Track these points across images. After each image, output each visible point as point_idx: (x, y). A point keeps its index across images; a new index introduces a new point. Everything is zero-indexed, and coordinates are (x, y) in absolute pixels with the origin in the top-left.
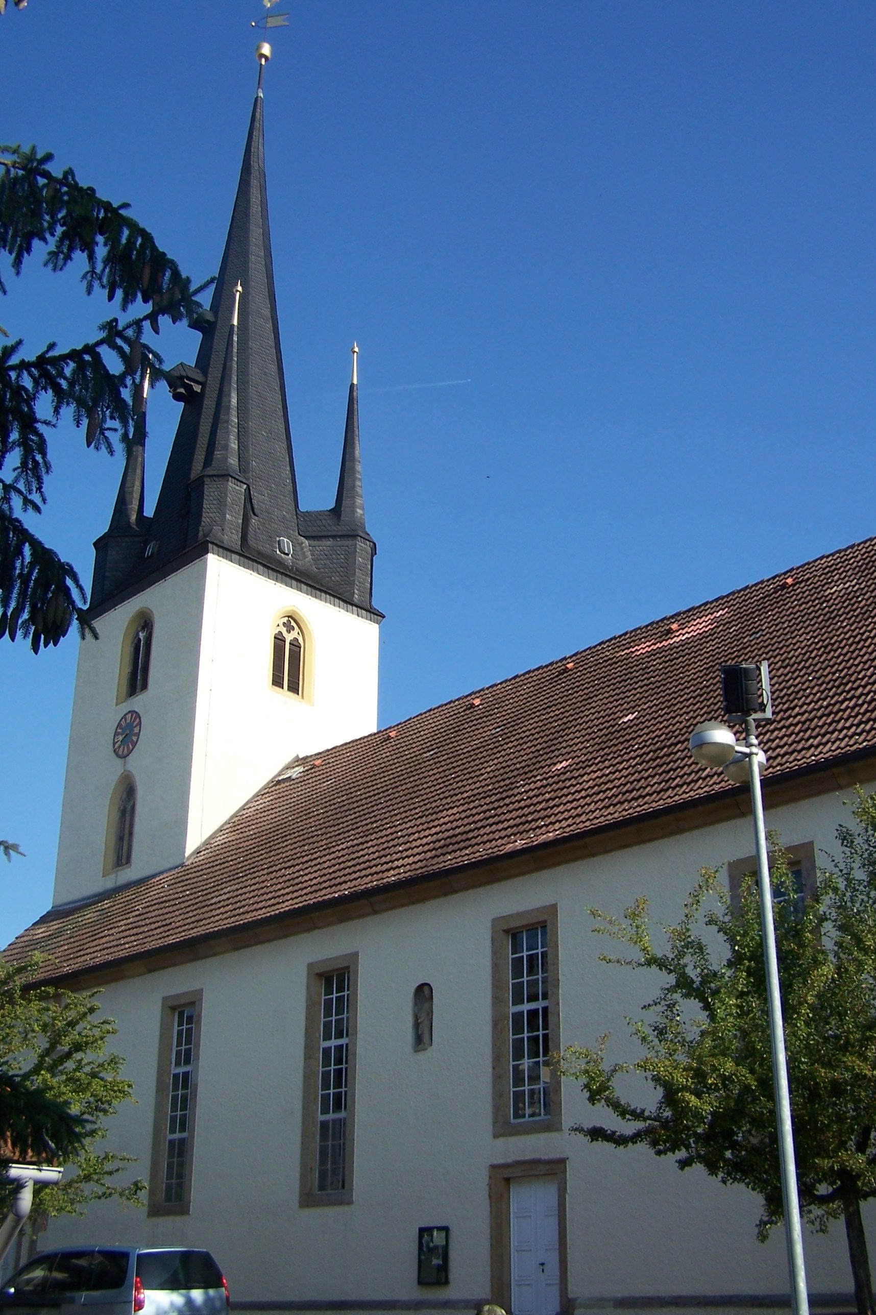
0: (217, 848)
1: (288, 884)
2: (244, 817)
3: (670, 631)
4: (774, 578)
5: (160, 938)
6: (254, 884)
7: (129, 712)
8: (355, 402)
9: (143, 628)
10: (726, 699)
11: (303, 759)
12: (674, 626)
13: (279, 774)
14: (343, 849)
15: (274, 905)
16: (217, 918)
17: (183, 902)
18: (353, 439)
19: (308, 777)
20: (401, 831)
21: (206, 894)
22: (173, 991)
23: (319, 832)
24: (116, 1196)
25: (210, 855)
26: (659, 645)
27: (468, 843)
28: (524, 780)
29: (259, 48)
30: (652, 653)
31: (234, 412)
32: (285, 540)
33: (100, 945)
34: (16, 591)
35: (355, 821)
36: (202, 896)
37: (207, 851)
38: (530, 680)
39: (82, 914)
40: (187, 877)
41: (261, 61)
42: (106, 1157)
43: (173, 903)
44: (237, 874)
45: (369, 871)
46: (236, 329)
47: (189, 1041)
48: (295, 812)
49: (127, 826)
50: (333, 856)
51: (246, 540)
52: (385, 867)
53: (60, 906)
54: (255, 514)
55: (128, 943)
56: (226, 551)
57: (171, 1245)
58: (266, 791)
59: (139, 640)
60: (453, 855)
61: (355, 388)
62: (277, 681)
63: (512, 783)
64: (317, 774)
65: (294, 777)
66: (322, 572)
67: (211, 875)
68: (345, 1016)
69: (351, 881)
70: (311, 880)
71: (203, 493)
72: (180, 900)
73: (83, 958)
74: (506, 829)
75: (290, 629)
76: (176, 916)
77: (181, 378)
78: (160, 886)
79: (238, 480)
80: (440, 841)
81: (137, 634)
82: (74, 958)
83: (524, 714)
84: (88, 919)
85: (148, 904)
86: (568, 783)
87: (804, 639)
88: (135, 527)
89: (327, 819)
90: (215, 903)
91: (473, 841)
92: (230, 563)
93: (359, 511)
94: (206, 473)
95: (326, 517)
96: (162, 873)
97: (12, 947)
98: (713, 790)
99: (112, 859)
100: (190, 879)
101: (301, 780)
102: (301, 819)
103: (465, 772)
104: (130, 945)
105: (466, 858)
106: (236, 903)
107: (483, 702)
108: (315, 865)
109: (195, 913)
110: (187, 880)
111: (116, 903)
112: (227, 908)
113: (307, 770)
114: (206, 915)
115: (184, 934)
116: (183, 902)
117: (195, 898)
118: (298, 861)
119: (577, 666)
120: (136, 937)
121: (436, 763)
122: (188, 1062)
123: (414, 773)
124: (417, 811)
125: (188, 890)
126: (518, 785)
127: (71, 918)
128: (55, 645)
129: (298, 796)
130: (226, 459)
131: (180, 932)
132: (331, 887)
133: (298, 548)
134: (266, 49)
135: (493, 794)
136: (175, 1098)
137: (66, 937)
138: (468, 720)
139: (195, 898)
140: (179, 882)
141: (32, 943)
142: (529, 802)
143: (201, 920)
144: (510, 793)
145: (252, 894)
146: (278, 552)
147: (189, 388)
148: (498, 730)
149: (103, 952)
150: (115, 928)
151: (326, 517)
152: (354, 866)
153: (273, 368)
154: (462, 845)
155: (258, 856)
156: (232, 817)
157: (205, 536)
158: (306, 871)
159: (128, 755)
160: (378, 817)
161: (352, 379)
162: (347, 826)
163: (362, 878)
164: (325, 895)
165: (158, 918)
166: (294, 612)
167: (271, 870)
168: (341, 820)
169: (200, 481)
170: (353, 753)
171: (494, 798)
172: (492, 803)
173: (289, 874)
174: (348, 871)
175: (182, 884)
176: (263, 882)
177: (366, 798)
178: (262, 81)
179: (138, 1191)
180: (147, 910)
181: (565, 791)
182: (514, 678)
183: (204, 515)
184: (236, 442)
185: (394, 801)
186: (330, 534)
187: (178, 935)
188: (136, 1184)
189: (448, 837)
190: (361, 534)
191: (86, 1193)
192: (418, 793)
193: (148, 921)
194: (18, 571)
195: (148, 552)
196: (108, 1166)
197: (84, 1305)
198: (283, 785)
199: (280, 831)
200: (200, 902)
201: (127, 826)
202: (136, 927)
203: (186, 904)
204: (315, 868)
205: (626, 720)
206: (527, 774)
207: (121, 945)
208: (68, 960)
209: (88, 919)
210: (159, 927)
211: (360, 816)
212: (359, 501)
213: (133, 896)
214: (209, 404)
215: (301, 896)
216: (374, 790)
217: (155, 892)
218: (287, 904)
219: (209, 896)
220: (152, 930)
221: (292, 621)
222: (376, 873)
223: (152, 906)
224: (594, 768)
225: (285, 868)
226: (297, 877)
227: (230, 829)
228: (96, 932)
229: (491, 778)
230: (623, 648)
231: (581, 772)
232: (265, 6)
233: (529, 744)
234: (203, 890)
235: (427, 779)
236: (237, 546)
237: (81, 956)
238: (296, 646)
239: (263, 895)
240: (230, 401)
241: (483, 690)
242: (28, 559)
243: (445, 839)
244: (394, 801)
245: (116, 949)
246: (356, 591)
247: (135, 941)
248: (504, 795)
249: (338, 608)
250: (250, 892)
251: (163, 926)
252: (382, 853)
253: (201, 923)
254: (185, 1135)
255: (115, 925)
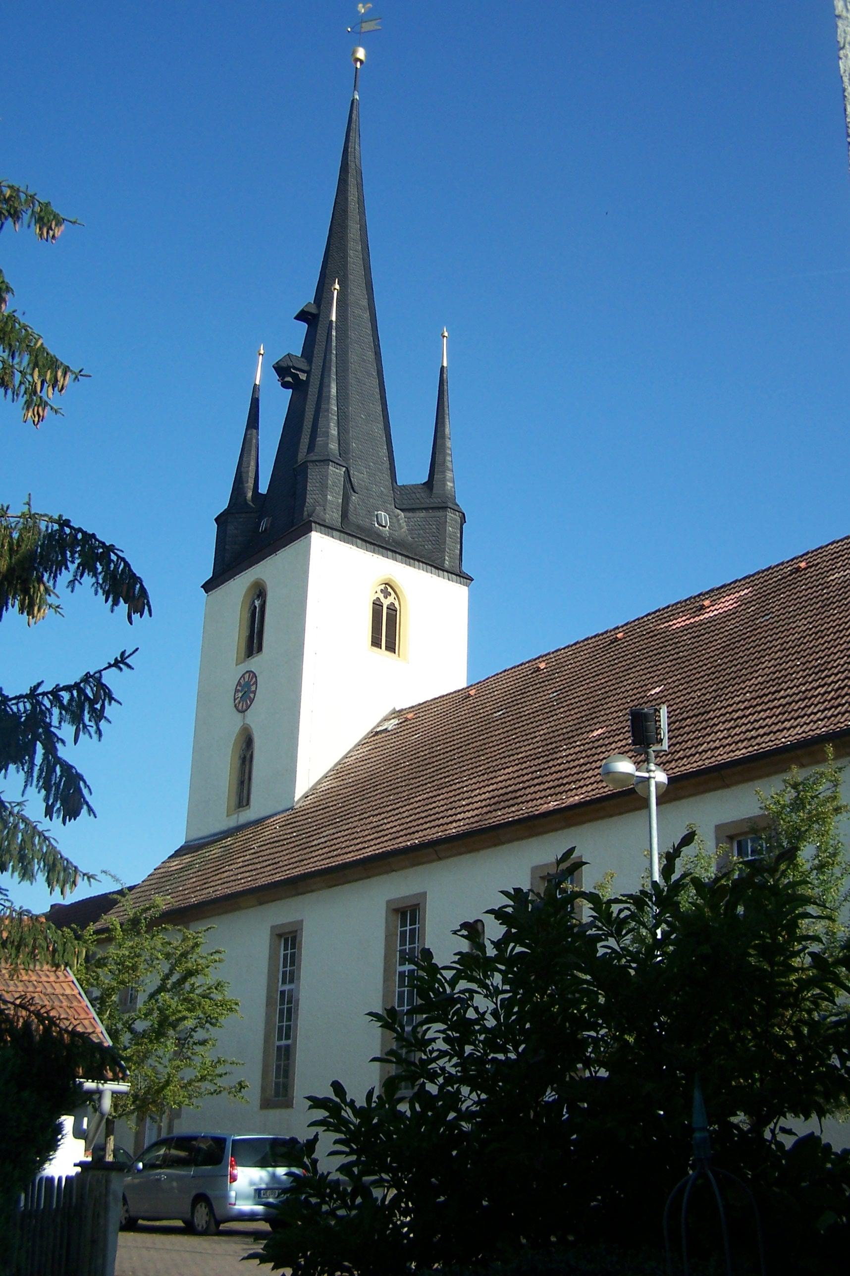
0: (322, 793)
1: (374, 830)
2: (346, 765)
3: (702, 607)
4: (792, 560)
5: (269, 876)
6: (348, 829)
7: (247, 672)
8: (445, 384)
9: (258, 596)
10: (633, 735)
11: (398, 711)
12: (707, 603)
13: (378, 726)
14: (420, 801)
15: (361, 849)
16: (316, 859)
17: (290, 843)
18: (444, 418)
19: (401, 730)
20: (466, 786)
21: (309, 837)
22: (284, 920)
23: (404, 784)
24: (224, 1094)
25: (316, 800)
26: (692, 620)
27: (516, 801)
28: (566, 745)
29: (354, 52)
30: (685, 628)
31: (333, 402)
32: (383, 513)
33: (221, 879)
34: (53, 792)
35: (432, 774)
36: (306, 838)
37: (313, 796)
38: (587, 647)
39: (209, 850)
40: (295, 820)
41: (356, 64)
42: (219, 1062)
43: (281, 843)
44: (335, 819)
45: (437, 822)
46: (334, 325)
47: (293, 963)
48: (386, 763)
49: (247, 771)
50: (411, 806)
51: (347, 516)
52: (450, 819)
53: (191, 841)
54: (355, 492)
55: (243, 878)
56: (328, 529)
57: (263, 1133)
58: (365, 741)
59: (255, 607)
60: (503, 811)
61: (445, 370)
62: (376, 643)
63: (557, 747)
64: (408, 727)
65: (390, 729)
66: (416, 542)
67: (314, 819)
68: (416, 945)
69: (422, 831)
70: (392, 828)
71: (307, 477)
72: (288, 841)
73: (207, 891)
74: (545, 790)
75: (387, 594)
76: (284, 855)
77: (289, 368)
78: (273, 827)
79: (337, 464)
80: (494, 797)
81: (254, 602)
82: (200, 890)
83: (629, 648)
84: (214, 854)
85: (262, 843)
86: (599, 750)
87: (802, 624)
88: (251, 504)
89: (411, 771)
90: (315, 845)
91: (520, 800)
92: (332, 539)
93: (450, 484)
94: (309, 459)
95: (419, 490)
96: (276, 814)
97: (151, 878)
98: (704, 764)
99: (234, 801)
100: (298, 821)
101: (395, 732)
102: (390, 770)
103: (523, 733)
104: (245, 880)
105: (511, 815)
106: (331, 846)
107: (548, 666)
108: (397, 814)
109: (298, 853)
110: (295, 822)
111: (237, 841)
112: (324, 850)
113: (401, 723)
114: (307, 856)
115: (288, 872)
116: (290, 843)
117: (300, 840)
118: (384, 810)
119: (626, 636)
120: (251, 873)
121: (502, 723)
122: (292, 981)
123: (484, 732)
124: (481, 768)
125: (295, 832)
126: (561, 749)
127: (200, 852)
128: (75, 819)
129: (391, 747)
130: (328, 444)
131: (285, 871)
132: (406, 835)
133: (395, 520)
134: (361, 53)
135: (542, 756)
136: (282, 1011)
137: (195, 870)
138: (533, 683)
139: (300, 840)
140: (289, 824)
141: (167, 874)
142: (567, 765)
143: (303, 860)
144: (555, 756)
145: (346, 838)
146: (376, 525)
147: (295, 377)
148: (555, 694)
149: (223, 886)
150: (234, 864)
151: (419, 490)
152: (426, 817)
153: (371, 355)
154: (511, 802)
155: (353, 803)
156: (336, 765)
157: (310, 515)
158: (389, 820)
159: (246, 710)
160: (451, 772)
161: (442, 363)
162: (426, 779)
163: (431, 828)
164: (401, 843)
165: (269, 857)
166: (390, 579)
167: (362, 816)
168: (422, 773)
169: (304, 467)
170: (439, 708)
171: (542, 760)
172: (539, 764)
173: (376, 821)
174: (421, 821)
175: (291, 826)
176: (354, 827)
177: (444, 753)
178: (358, 83)
179: (242, 1090)
180: (262, 848)
181: (596, 757)
182: (575, 644)
183: (308, 496)
184: (336, 428)
185: (465, 758)
186: (422, 506)
187: (284, 873)
188: (240, 1083)
189: (501, 795)
190: (450, 505)
191: (203, 1090)
192: (485, 751)
193: (261, 859)
194: (53, 782)
195: (263, 526)
196: (220, 1070)
197: (193, 1177)
198: (380, 736)
199: (373, 780)
200: (304, 843)
201: (247, 771)
202: (251, 864)
203: (292, 845)
204: (397, 817)
205: (653, 692)
206: (569, 739)
207: (238, 880)
208: (195, 892)
209: (214, 854)
210: (269, 865)
211: (437, 770)
212: (449, 475)
213: (251, 835)
214: (313, 390)
215: (383, 842)
216: (451, 746)
217: (269, 833)
218: (371, 849)
219: (311, 839)
220: (263, 867)
221: (389, 588)
222: (442, 825)
223: (265, 845)
224: (621, 737)
225: (373, 816)
226: (382, 825)
227: (334, 777)
228: (219, 867)
229: (542, 741)
230: (664, 620)
231: (611, 740)
232: (360, 12)
233: (576, 710)
234: (307, 833)
235: (494, 739)
236: (338, 524)
237: (206, 888)
238: (392, 609)
239: (353, 839)
240: (330, 391)
241: (549, 654)
242: (59, 773)
243: (499, 796)
244: (465, 758)
245: (233, 883)
246: (447, 558)
247: (249, 877)
248: (550, 757)
249: (430, 574)
250: (343, 836)
251: (273, 864)
252: (450, 806)
253: (303, 863)
254: (289, 1042)
255: (235, 861)
